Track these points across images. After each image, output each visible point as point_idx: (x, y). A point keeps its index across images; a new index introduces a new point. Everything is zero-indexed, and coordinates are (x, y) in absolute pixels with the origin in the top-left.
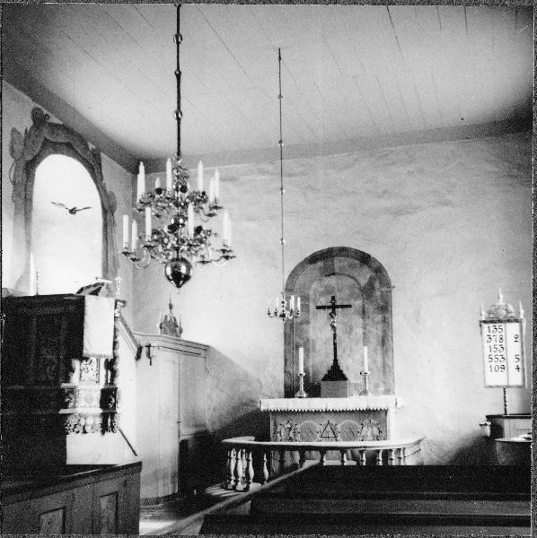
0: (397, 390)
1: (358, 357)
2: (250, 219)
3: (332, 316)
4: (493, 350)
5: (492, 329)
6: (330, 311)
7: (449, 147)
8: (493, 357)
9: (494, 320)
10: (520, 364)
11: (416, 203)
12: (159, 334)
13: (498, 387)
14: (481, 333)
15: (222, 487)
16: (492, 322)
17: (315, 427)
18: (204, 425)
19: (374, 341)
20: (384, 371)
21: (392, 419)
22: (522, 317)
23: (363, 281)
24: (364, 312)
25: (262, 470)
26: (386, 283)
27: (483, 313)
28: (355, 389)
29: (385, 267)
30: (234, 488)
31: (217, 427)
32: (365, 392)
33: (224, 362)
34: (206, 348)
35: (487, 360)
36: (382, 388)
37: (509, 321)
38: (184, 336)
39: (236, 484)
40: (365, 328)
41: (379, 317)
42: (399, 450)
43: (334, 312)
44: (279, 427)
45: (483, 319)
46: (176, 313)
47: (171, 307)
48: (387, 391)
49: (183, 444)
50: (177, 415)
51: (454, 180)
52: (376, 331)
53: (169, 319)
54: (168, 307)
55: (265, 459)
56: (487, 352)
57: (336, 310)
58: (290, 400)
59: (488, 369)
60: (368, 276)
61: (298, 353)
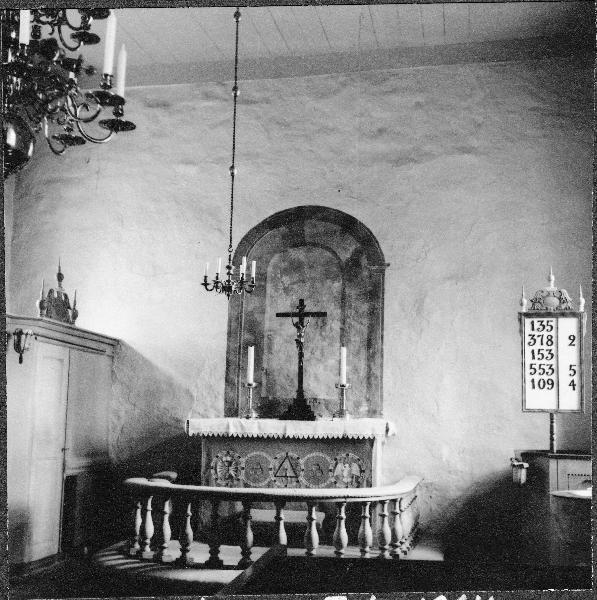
0: (384, 412)
1: (332, 362)
2: (188, 162)
3: (299, 326)
4: (537, 356)
5: (537, 325)
6: (296, 320)
7: (467, 72)
8: (537, 367)
9: (538, 311)
10: (576, 378)
11: (427, 148)
12: (39, 316)
13: (543, 411)
14: (521, 332)
15: (120, 551)
16: (538, 315)
17: (268, 462)
18: (106, 453)
19: (357, 339)
20: (369, 384)
21: (380, 454)
22: (582, 309)
23: (345, 256)
24: (343, 298)
25: (185, 527)
26: (378, 260)
27: (525, 301)
28: (327, 408)
29: (378, 238)
30: (139, 555)
31: (125, 456)
32: (341, 413)
33: (136, 361)
34: (115, 343)
35: (528, 370)
36: (364, 408)
37: (563, 315)
38: (80, 323)
39: (142, 549)
40: (344, 322)
41: (365, 307)
42: (394, 501)
43: (301, 322)
44: (215, 459)
45: (524, 310)
46: (68, 288)
47: (60, 277)
48: (373, 413)
49: (69, 483)
50: (62, 439)
51: (480, 119)
52: (359, 329)
53: (56, 295)
54: (56, 277)
55: (189, 512)
56: (528, 360)
57: (306, 319)
58: (232, 421)
59: (529, 385)
60: (352, 249)
61: (246, 354)
